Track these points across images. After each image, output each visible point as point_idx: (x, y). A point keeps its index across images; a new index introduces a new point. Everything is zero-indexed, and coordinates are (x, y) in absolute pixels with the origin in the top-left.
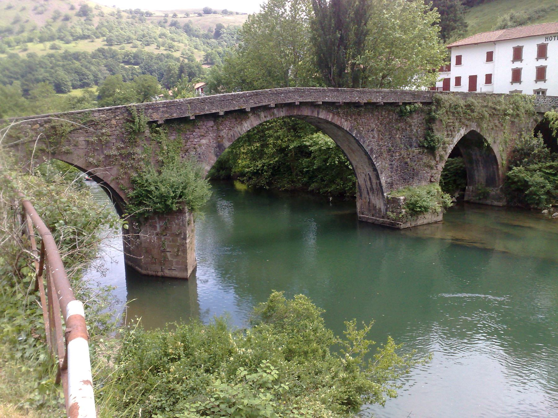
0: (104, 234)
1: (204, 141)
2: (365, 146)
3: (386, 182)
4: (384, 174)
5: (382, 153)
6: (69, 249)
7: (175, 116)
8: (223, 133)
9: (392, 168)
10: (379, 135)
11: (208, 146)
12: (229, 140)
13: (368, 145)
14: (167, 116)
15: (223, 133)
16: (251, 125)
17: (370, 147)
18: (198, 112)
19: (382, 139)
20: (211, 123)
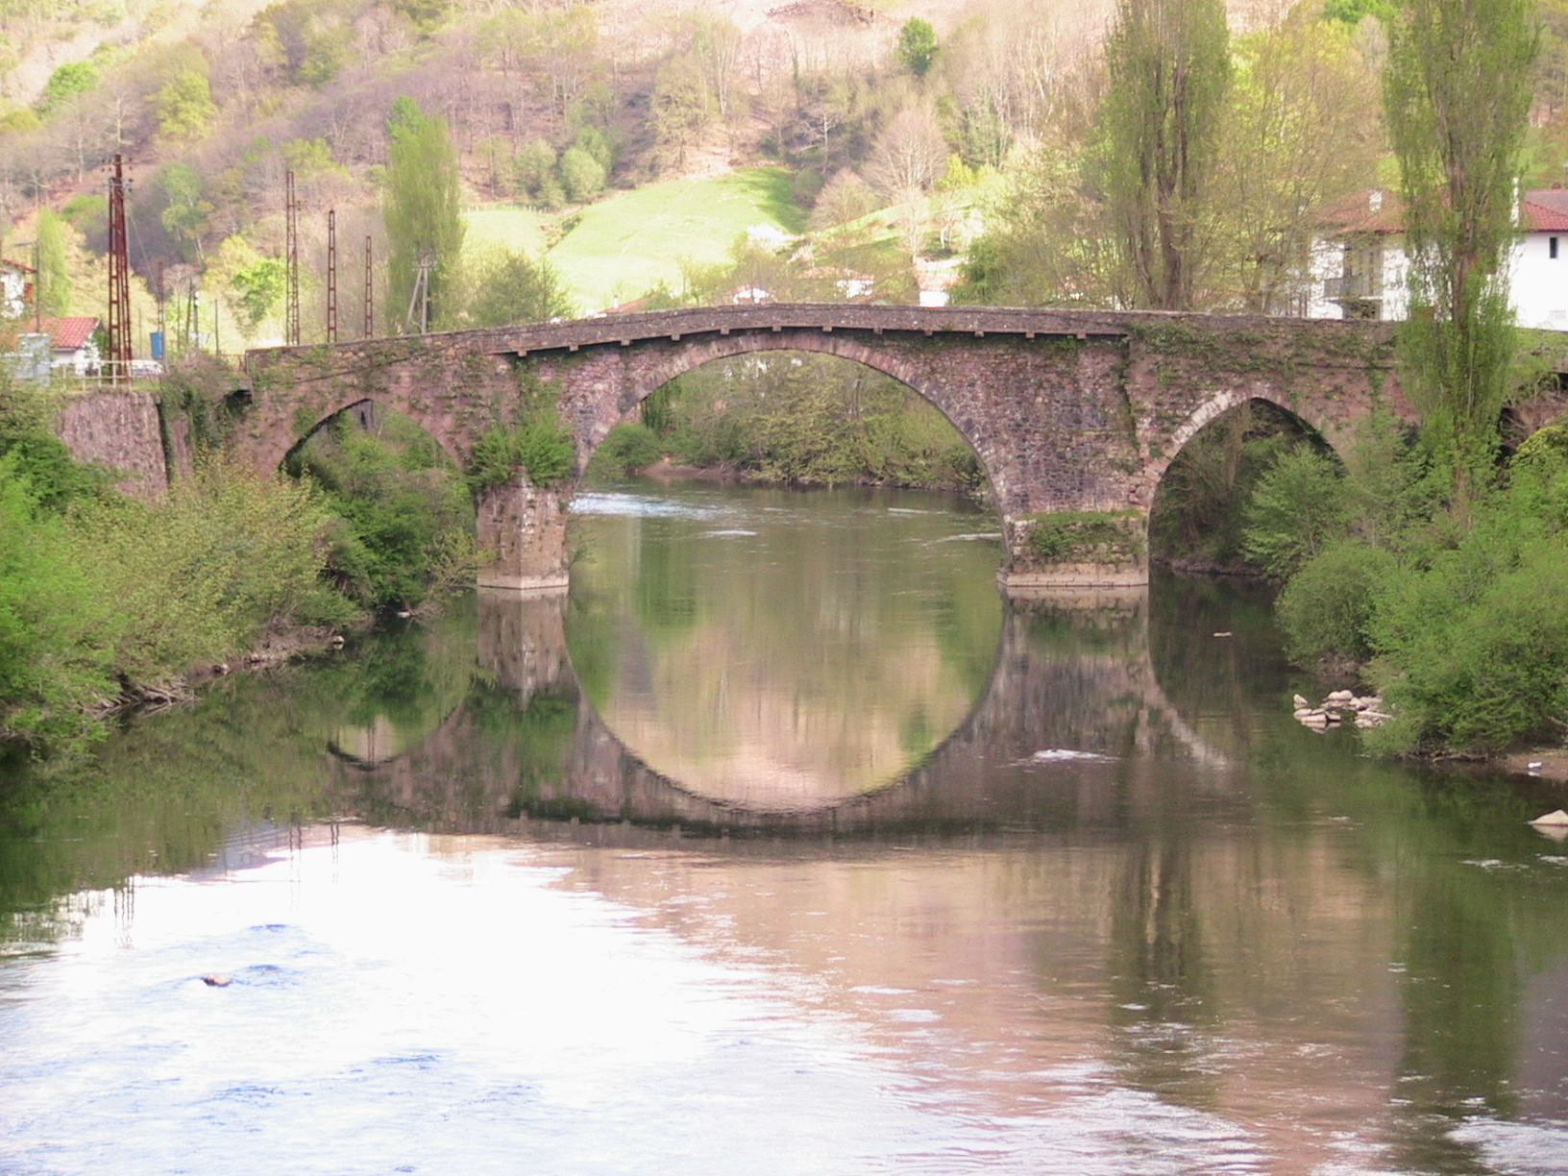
0: (115, 108)
1: (599, 386)
2: (951, 413)
3: (1009, 491)
4: (1002, 476)
5: (996, 432)
6: (168, 1049)
7: (545, 345)
8: (637, 374)
9: (1024, 464)
10: (988, 396)
11: (607, 393)
12: (646, 386)
13: (961, 414)
14: (533, 346)
15: (637, 374)
16: (691, 363)
17: (964, 418)
18: (583, 340)
19: (997, 404)
20: (615, 358)
